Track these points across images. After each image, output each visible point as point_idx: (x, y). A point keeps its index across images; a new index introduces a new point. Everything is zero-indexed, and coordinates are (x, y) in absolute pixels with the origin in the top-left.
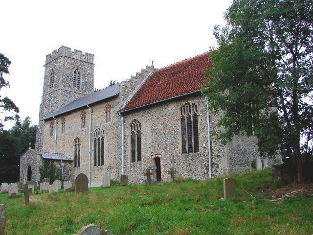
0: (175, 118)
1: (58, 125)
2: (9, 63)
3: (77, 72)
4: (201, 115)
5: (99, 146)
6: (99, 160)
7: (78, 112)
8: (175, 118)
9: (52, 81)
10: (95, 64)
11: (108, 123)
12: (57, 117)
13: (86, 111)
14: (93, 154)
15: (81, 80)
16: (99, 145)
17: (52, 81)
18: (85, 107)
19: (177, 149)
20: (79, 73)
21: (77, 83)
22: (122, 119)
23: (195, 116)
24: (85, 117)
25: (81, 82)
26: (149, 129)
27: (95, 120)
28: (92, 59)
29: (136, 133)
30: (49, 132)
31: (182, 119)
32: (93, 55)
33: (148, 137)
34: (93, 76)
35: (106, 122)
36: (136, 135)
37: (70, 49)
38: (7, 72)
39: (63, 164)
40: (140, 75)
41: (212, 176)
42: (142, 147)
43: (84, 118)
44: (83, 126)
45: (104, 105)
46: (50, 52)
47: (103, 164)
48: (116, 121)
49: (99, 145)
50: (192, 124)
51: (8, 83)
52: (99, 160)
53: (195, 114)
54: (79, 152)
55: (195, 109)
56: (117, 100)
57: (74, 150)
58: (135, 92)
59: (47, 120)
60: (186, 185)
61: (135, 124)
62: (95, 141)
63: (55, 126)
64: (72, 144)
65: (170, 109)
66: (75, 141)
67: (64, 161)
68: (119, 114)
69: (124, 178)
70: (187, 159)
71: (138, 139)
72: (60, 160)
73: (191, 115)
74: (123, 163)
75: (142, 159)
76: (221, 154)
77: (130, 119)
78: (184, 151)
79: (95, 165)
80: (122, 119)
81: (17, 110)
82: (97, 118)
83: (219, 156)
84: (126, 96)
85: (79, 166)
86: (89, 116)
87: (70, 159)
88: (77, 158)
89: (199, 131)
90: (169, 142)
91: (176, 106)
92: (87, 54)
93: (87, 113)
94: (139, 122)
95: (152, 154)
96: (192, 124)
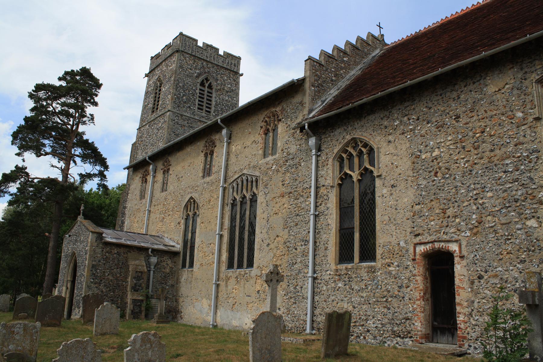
0: (520, 114)
2: (99, 86)
3: (207, 85)
5: (241, 239)
7: (198, 144)
9: (157, 99)
10: (242, 75)
11: (270, 158)
13: (216, 137)
14: (226, 239)
15: (213, 99)
17: (157, 99)
18: (215, 128)
20: (210, 87)
22: (312, 141)
24: (212, 153)
25: (214, 103)
27: (237, 156)
29: (355, 176)
30: (138, 192)
32: (239, 59)
33: (402, 186)
35: (265, 156)
36: (356, 186)
38: (95, 104)
39: (154, 260)
42: (378, 217)
43: (209, 154)
44: (207, 171)
47: (250, 264)
48: (293, 149)
50: (357, 236)
51: (93, 119)
54: (193, 233)
56: (297, 99)
57: (182, 227)
58: (343, 83)
62: (233, 205)
63: (150, 179)
64: (179, 216)
65: (491, 89)
66: (186, 206)
71: (363, 195)
74: (310, 265)
75: (378, 256)
79: (230, 266)
80: (312, 141)
85: (191, 265)
87: (173, 249)
92: (228, 55)
93: (217, 143)
94: (365, 145)
95: (418, 240)
96: (357, 236)
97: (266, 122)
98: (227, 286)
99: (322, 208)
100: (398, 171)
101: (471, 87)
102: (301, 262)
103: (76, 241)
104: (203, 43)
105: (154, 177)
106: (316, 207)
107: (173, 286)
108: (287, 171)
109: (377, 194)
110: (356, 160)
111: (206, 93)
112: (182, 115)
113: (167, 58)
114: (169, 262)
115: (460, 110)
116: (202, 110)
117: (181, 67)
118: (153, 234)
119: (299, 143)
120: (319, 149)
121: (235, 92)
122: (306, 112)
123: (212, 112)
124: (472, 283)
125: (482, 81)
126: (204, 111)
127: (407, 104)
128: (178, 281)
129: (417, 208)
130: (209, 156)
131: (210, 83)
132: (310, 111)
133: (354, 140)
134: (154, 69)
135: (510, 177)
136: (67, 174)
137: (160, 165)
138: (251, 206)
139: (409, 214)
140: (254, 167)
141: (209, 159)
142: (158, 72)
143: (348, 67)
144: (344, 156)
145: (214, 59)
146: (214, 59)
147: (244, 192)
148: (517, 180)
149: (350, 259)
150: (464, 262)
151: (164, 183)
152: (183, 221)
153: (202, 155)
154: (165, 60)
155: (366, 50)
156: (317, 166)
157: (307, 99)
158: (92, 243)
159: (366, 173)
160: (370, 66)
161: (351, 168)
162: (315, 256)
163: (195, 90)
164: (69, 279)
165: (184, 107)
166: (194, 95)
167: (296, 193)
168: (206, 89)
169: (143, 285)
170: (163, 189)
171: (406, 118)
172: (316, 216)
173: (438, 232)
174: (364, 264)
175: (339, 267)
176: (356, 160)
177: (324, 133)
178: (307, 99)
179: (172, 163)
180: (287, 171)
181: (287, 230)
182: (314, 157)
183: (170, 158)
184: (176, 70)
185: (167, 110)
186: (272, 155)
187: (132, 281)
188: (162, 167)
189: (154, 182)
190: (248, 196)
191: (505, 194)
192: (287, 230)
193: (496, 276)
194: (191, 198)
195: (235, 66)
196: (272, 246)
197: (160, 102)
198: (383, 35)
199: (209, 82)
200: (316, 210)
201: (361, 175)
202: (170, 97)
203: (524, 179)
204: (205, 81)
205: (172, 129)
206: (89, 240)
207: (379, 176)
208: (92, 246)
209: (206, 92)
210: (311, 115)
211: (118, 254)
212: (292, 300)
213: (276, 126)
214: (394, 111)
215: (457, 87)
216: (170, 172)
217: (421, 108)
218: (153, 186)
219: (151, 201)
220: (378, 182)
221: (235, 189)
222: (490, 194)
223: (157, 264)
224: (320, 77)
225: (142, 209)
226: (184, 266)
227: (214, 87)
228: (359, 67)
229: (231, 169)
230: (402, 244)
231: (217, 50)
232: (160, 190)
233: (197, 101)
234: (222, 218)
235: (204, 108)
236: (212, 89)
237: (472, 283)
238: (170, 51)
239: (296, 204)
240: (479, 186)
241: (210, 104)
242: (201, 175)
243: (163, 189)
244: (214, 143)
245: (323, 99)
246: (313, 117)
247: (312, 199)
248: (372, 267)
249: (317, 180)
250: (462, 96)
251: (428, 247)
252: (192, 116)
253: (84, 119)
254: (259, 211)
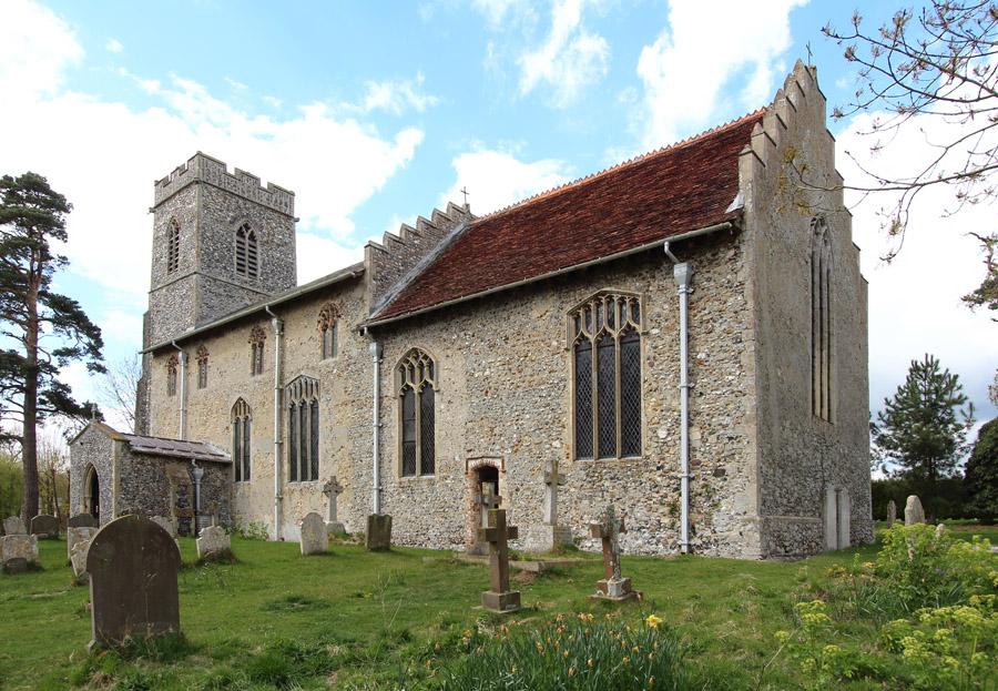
0: (554, 343)
1: (187, 370)
3: (247, 235)
4: (655, 331)
6: (302, 463)
7: (243, 331)
8: (554, 343)
9: (173, 251)
10: (297, 220)
11: (330, 360)
12: (185, 342)
13: (264, 325)
15: (259, 257)
16: (302, 413)
17: (173, 251)
18: (261, 316)
19: (556, 444)
20: (252, 237)
21: (246, 264)
23: (630, 336)
24: (262, 345)
25: (260, 262)
26: (461, 381)
28: (290, 204)
31: (576, 346)
32: (293, 195)
33: (457, 403)
34: (293, 250)
37: (224, 165)
39: (199, 472)
40: (431, 228)
41: (690, 538)
43: (258, 347)
44: (258, 368)
45: (317, 310)
46: (164, 171)
47: (315, 476)
49: (302, 413)
50: (418, 450)
52: (302, 463)
53: (630, 330)
54: (247, 439)
55: (629, 313)
56: (357, 293)
57: (232, 433)
58: (413, 273)
59: (162, 351)
60: (881, 531)
61: (416, 365)
62: (292, 410)
63: (180, 369)
64: (226, 420)
65: (535, 314)
66: (235, 408)
67: (200, 462)
68: (362, 332)
69: (380, 526)
70: (593, 478)
72: (188, 460)
73: (615, 335)
75: (437, 469)
76: (729, 467)
77: (399, 348)
78: (581, 450)
79: (293, 478)
81: (93, 332)
82: (299, 344)
83: (719, 473)
84: (384, 282)
85: (247, 477)
86: (272, 345)
88: (242, 453)
89: (644, 388)
90: (528, 421)
91: (558, 304)
92: (274, 189)
93: (267, 333)
94: (426, 357)
96: (418, 450)
97: (324, 315)
98: (291, 500)
99: (385, 419)
100: (455, 387)
101: (519, 309)
102: (367, 474)
103: (92, 450)
104: (236, 169)
105: (186, 367)
106: (380, 418)
107: (225, 501)
108: (350, 376)
109: (436, 409)
110: (417, 372)
111: (247, 246)
112: (215, 280)
113: (183, 188)
114: (219, 474)
115: (509, 332)
116: (244, 271)
117: (205, 206)
118: (194, 440)
119: (360, 346)
120: (381, 356)
121: (289, 269)
122: (367, 310)
123: (259, 275)
124: (511, 495)
125: (528, 305)
126: (247, 273)
127: (464, 318)
128: (232, 496)
129: (470, 425)
130: (258, 349)
131: (252, 232)
132: (372, 311)
133: (415, 350)
134: (163, 203)
135: (544, 401)
136: (36, 348)
137: (193, 353)
138: (313, 412)
139: (463, 431)
140: (313, 368)
141: (258, 353)
142: (168, 207)
143: (419, 253)
144: (406, 366)
145: (254, 194)
146: (254, 194)
147: (304, 396)
148: (548, 405)
149: (413, 472)
150: (505, 477)
151: (201, 378)
152: (232, 427)
153: (250, 346)
154: (179, 191)
155: (444, 227)
156: (380, 375)
157: (368, 297)
158: (116, 452)
159: (426, 387)
160: (446, 250)
161: (413, 381)
162: (379, 468)
163: (230, 243)
164: (87, 496)
165: (217, 267)
166: (229, 250)
167: (359, 403)
168: (247, 241)
169: (189, 501)
170: (202, 384)
171: (462, 333)
172: (380, 428)
173: (486, 448)
174: (424, 477)
175: (404, 479)
176: (417, 372)
177: (386, 339)
178: (368, 297)
179: (209, 351)
180: (350, 376)
181: (351, 441)
182: (376, 365)
183: (206, 345)
184: (198, 212)
185: (193, 272)
186: (332, 356)
187: (174, 496)
188: (196, 356)
189: (187, 375)
190: (308, 401)
191: (539, 417)
192: (351, 441)
193: (528, 489)
194: (240, 399)
195: (286, 205)
196: (337, 457)
197: (180, 258)
198: (467, 205)
199: (250, 231)
200: (379, 421)
201: (422, 388)
202: (194, 251)
203: (554, 405)
204: (244, 230)
205: (203, 299)
206: (113, 450)
207: (437, 391)
208: (117, 456)
209: (247, 245)
210: (372, 317)
211: (153, 465)
212: (360, 512)
213: (335, 322)
214: (453, 323)
215: (508, 307)
216: (209, 364)
217: (476, 324)
218: (186, 379)
219: (186, 399)
220: (437, 396)
221: (293, 392)
222: (528, 416)
223: (204, 476)
224: (383, 268)
225: (174, 408)
226: (238, 479)
227: (258, 238)
228: (434, 251)
229: (289, 368)
230: (457, 458)
231: (257, 180)
232: (196, 385)
233: (235, 258)
235: (247, 268)
236: (255, 241)
237: (511, 495)
238: (185, 180)
239: (360, 414)
240: (519, 408)
241: (255, 264)
242: (250, 371)
243: (202, 384)
244: (263, 334)
245: (388, 294)
246: (376, 319)
247: (375, 410)
248: (432, 479)
249: (380, 390)
250: (512, 317)
251: (478, 462)
252: (230, 281)
253: (51, 263)
254: (321, 419)
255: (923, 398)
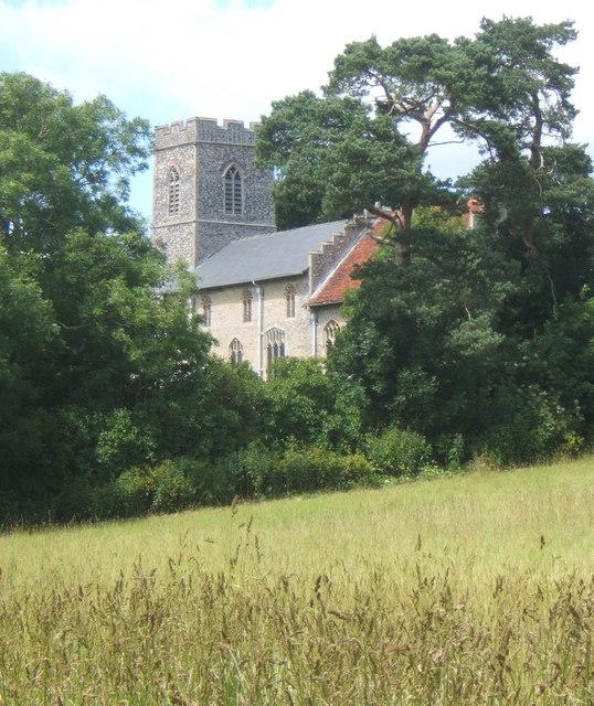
11: (291, 319)
20: (238, 177)
24: (249, 302)
25: (243, 198)
44: (247, 318)
45: (285, 285)
62: (269, 349)
66: (231, 346)
86: (256, 305)
163: (220, 188)
227: (243, 177)
234: (262, 358)
255: (433, 668)
